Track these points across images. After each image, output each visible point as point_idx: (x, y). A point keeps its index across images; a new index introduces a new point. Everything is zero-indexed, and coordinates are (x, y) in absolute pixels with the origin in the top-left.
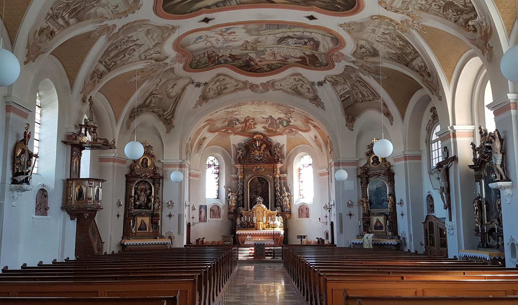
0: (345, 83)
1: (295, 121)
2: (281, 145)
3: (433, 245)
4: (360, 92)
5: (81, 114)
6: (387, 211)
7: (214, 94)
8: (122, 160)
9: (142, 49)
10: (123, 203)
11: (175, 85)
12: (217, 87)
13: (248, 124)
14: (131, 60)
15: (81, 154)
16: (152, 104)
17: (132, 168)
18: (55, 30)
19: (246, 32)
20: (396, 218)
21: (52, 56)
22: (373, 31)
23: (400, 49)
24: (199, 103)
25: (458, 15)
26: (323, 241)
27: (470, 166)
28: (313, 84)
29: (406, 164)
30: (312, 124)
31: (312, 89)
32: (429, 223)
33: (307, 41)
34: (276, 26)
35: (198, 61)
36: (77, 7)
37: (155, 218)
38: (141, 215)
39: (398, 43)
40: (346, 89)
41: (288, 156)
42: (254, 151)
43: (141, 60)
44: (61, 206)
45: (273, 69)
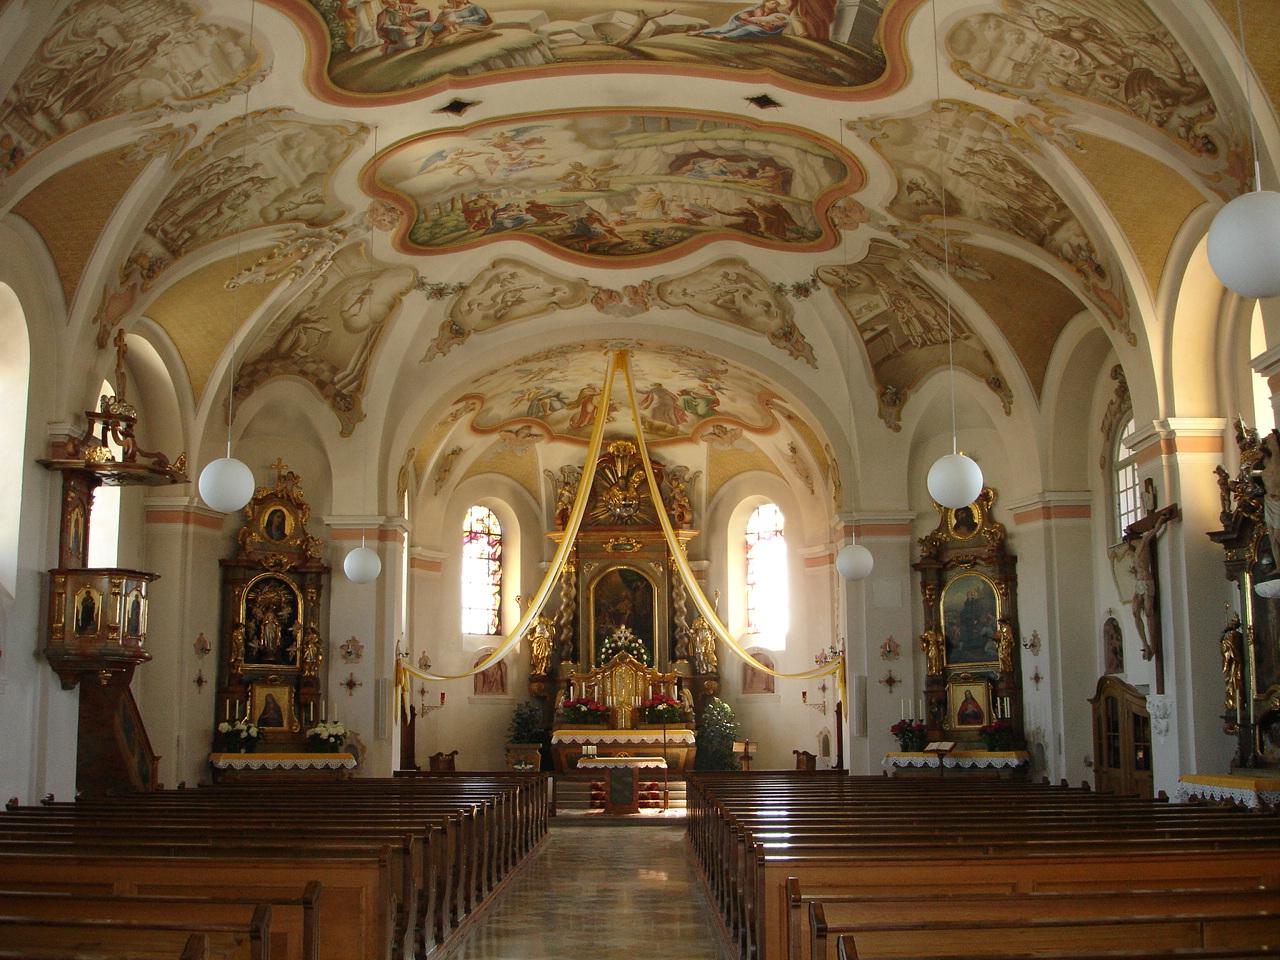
0: (873, 288)
1: (733, 400)
2: (692, 469)
3: (1117, 764)
4: (918, 317)
5: (93, 385)
6: (997, 667)
7: (485, 317)
8: (206, 518)
9: (271, 192)
10: (212, 638)
11: (367, 292)
12: (493, 299)
13: (590, 408)
14: (237, 223)
15: (90, 498)
16: (299, 351)
17: (238, 543)
18: (25, 145)
19: (578, 139)
20: (1021, 688)
21: (16, 220)
22: (942, 143)
23: (1019, 195)
24: (440, 347)
25: (1166, 105)
26: (811, 759)
27: (1213, 535)
28: (780, 289)
29: (1048, 530)
30: (782, 410)
31: (780, 305)
32: (1107, 699)
33: (754, 165)
34: (663, 122)
35: (436, 224)
36: (86, 81)
37: (307, 690)
38: (264, 680)
39: (1013, 179)
40: (877, 306)
41: (712, 506)
42: (608, 490)
43: (267, 223)
44: (33, 647)
45: (657, 246)
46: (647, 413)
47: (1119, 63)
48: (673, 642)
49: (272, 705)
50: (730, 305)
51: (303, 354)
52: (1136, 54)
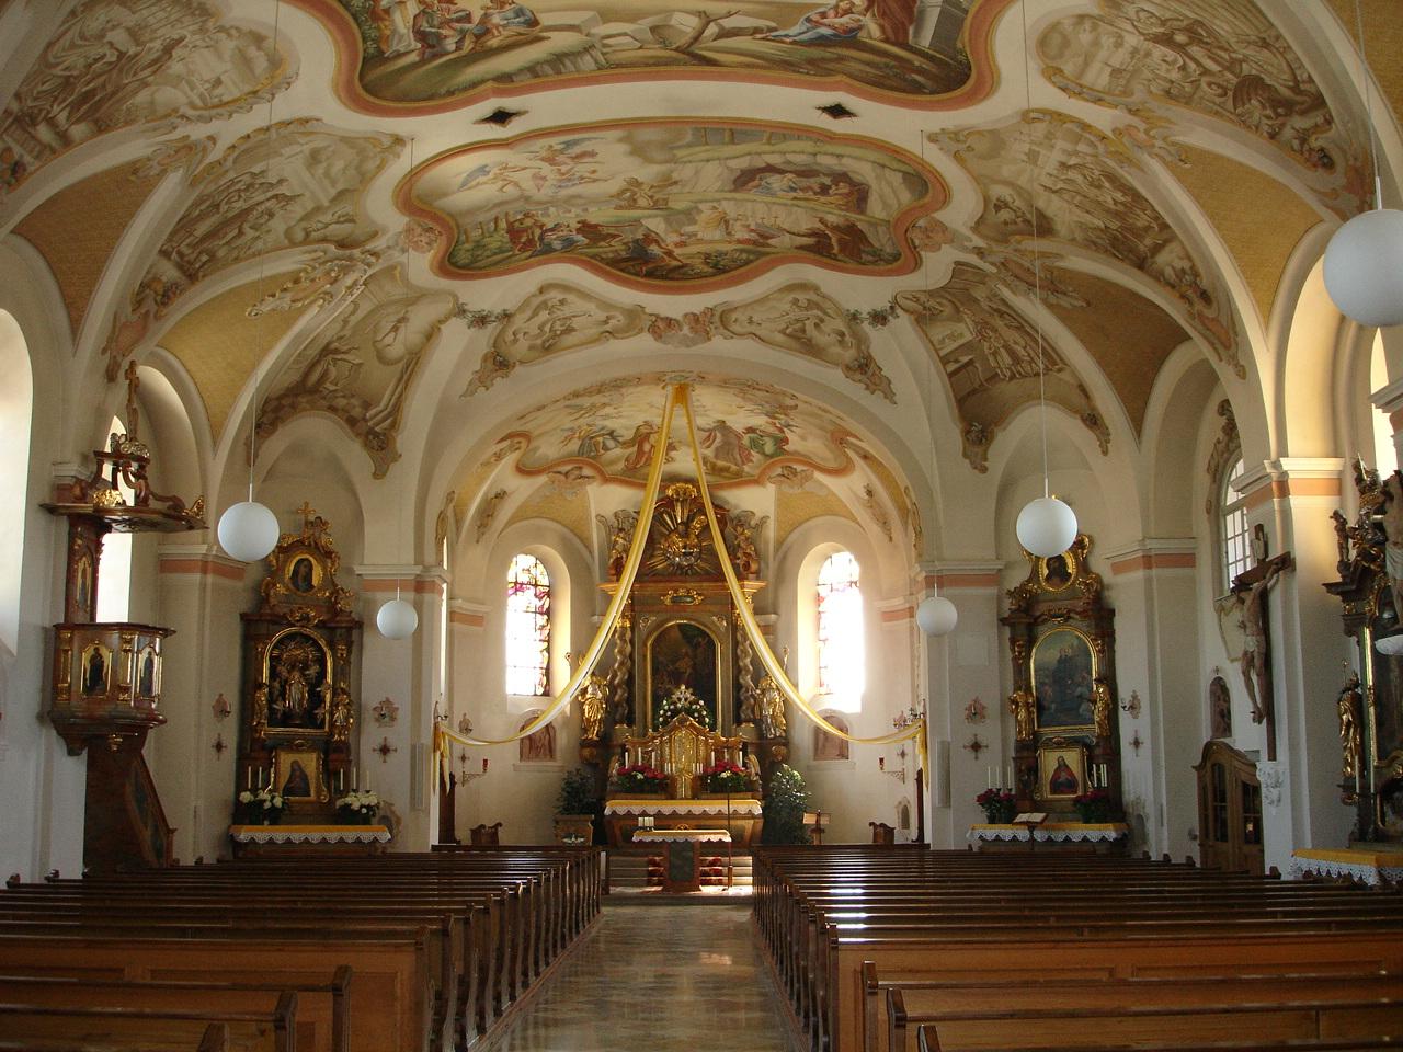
0: (957, 316)
1: (803, 438)
2: (759, 514)
3: (1224, 838)
4: (1007, 347)
5: (102, 422)
6: (1093, 731)
7: (531, 348)
8: (226, 567)
9: (297, 210)
10: (232, 700)
11: (403, 320)
12: (541, 328)
13: (647, 447)
14: (259, 245)
15: (98, 546)
16: (328, 385)
17: (261, 595)
18: (28, 159)
19: (633, 153)
20: (1119, 754)
21: (17, 241)
22: (1032, 157)
23: (1116, 214)
24: (482, 380)
25: (1278, 115)
26: (889, 831)
27: (1330, 587)
28: (855, 317)
29: (1149, 580)
30: (857, 450)
31: (854, 335)
32: (1213, 766)
33: (827, 181)
34: (727, 134)
35: (478, 245)
36: (94, 89)
37: (337, 756)
38: (289, 745)
39: (1110, 196)
40: (961, 335)
41: (780, 554)
42: (667, 537)
43: (293, 244)
44: (36, 709)
45: (720, 269)
46: (710, 453)
47: (1227, 69)
48: (738, 704)
49: (298, 773)
50: (800, 334)
51: (332, 388)
52: (1246, 59)
